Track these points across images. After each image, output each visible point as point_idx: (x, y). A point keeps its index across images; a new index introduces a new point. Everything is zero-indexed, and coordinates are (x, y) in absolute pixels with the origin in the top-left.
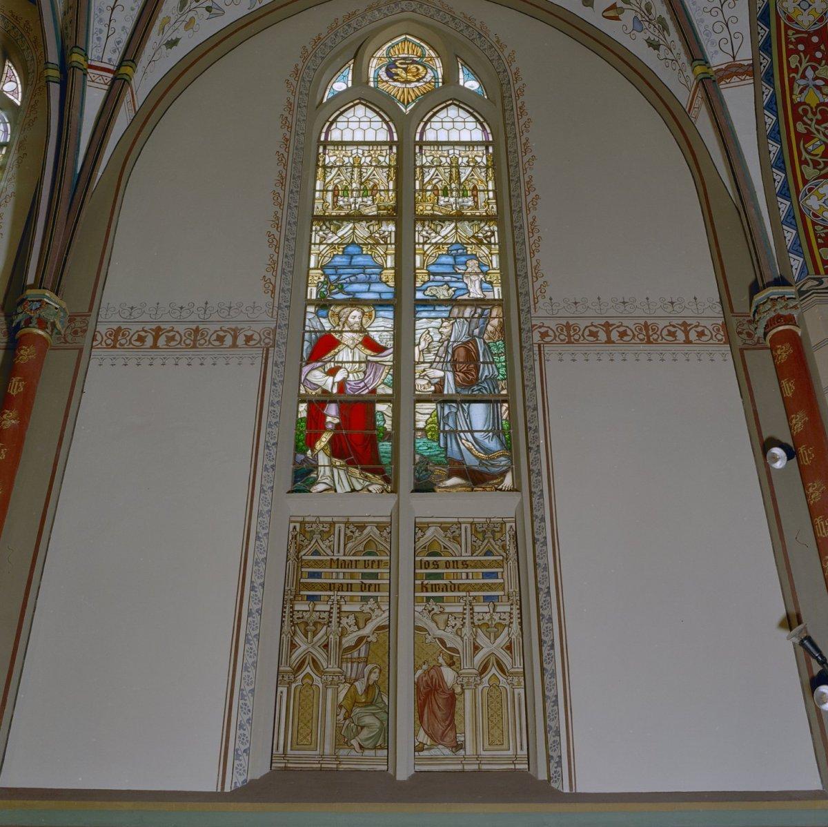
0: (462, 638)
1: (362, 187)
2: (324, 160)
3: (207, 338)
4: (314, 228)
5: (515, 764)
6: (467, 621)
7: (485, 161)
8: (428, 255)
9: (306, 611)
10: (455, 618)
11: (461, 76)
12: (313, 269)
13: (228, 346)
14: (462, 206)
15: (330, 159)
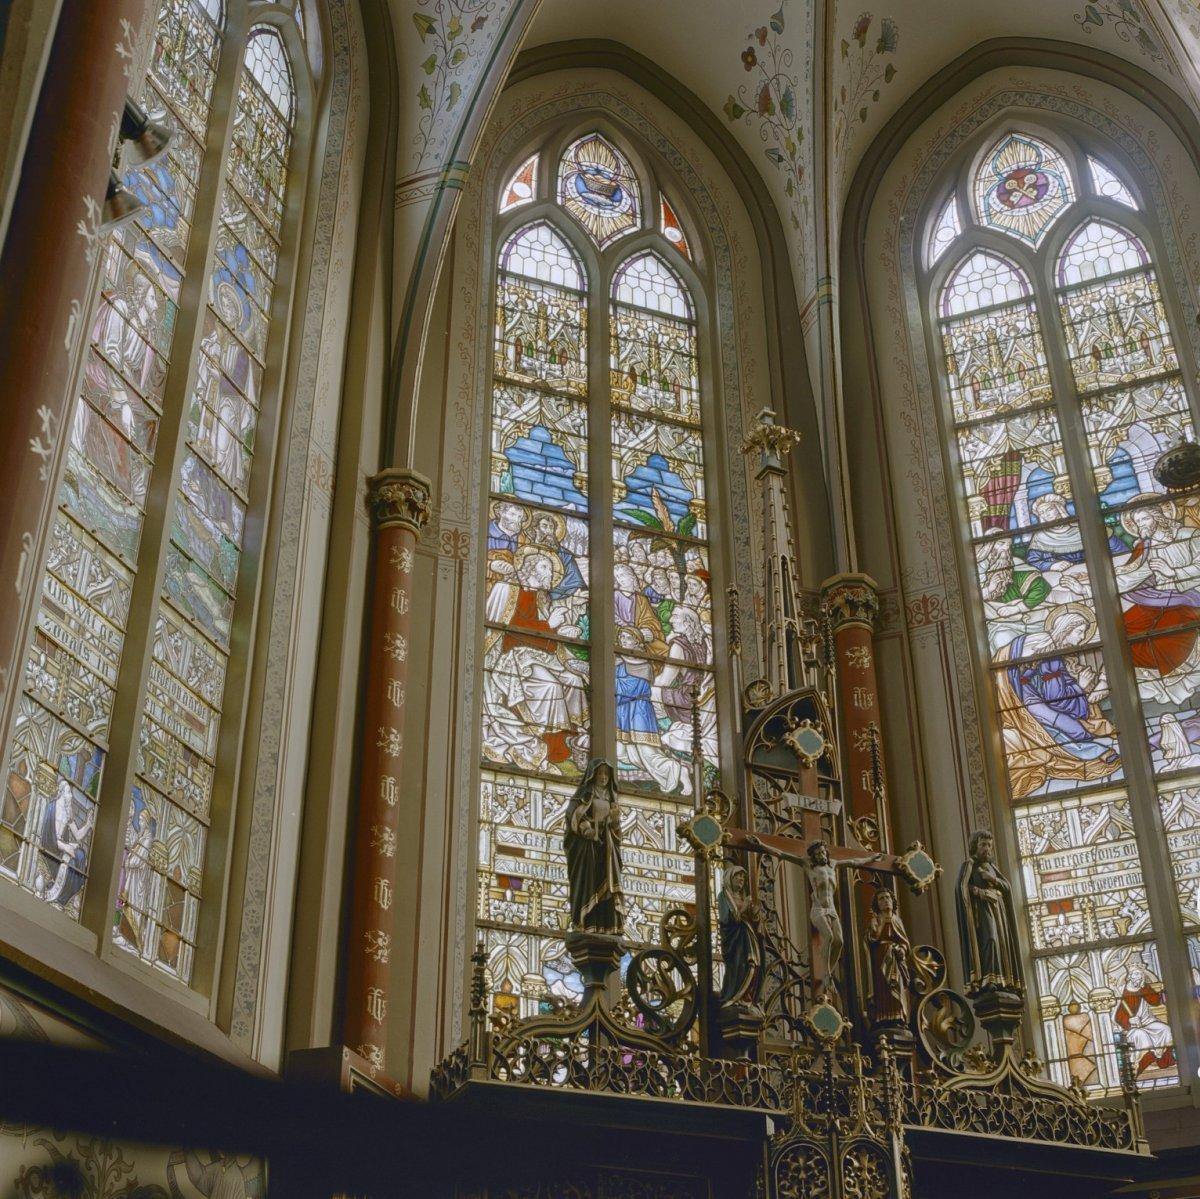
7: (1148, 295)
15: (1075, 312)
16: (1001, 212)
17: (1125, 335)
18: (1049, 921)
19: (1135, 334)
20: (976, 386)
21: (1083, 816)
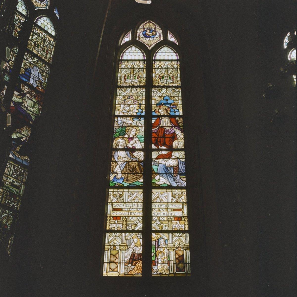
1: (134, 76)
2: (121, 66)
7: (177, 67)
11: (169, 36)
14: (169, 82)
16: (142, 38)
18: (113, 221)
19: (171, 75)
20: (125, 78)
21: (129, 194)
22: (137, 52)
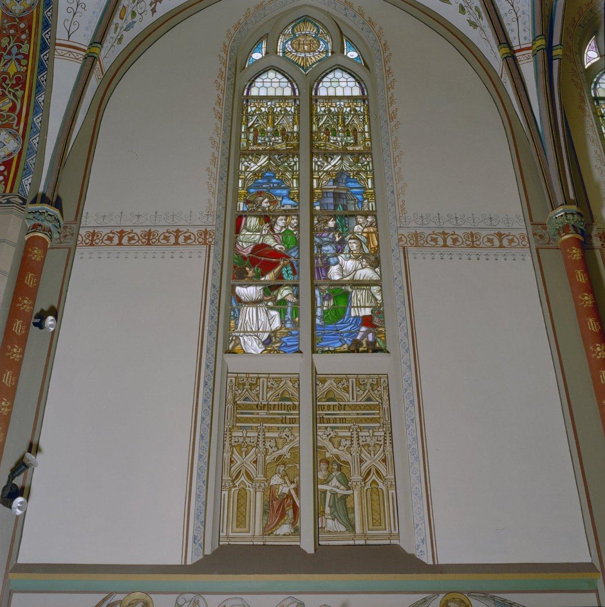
0: (351, 455)
3: (157, 238)
4: (314, 160)
5: (390, 540)
6: (355, 442)
8: (322, 179)
9: (241, 437)
10: (346, 440)
12: (316, 189)
13: (172, 244)
17: (274, 127)
22: (280, 82)
